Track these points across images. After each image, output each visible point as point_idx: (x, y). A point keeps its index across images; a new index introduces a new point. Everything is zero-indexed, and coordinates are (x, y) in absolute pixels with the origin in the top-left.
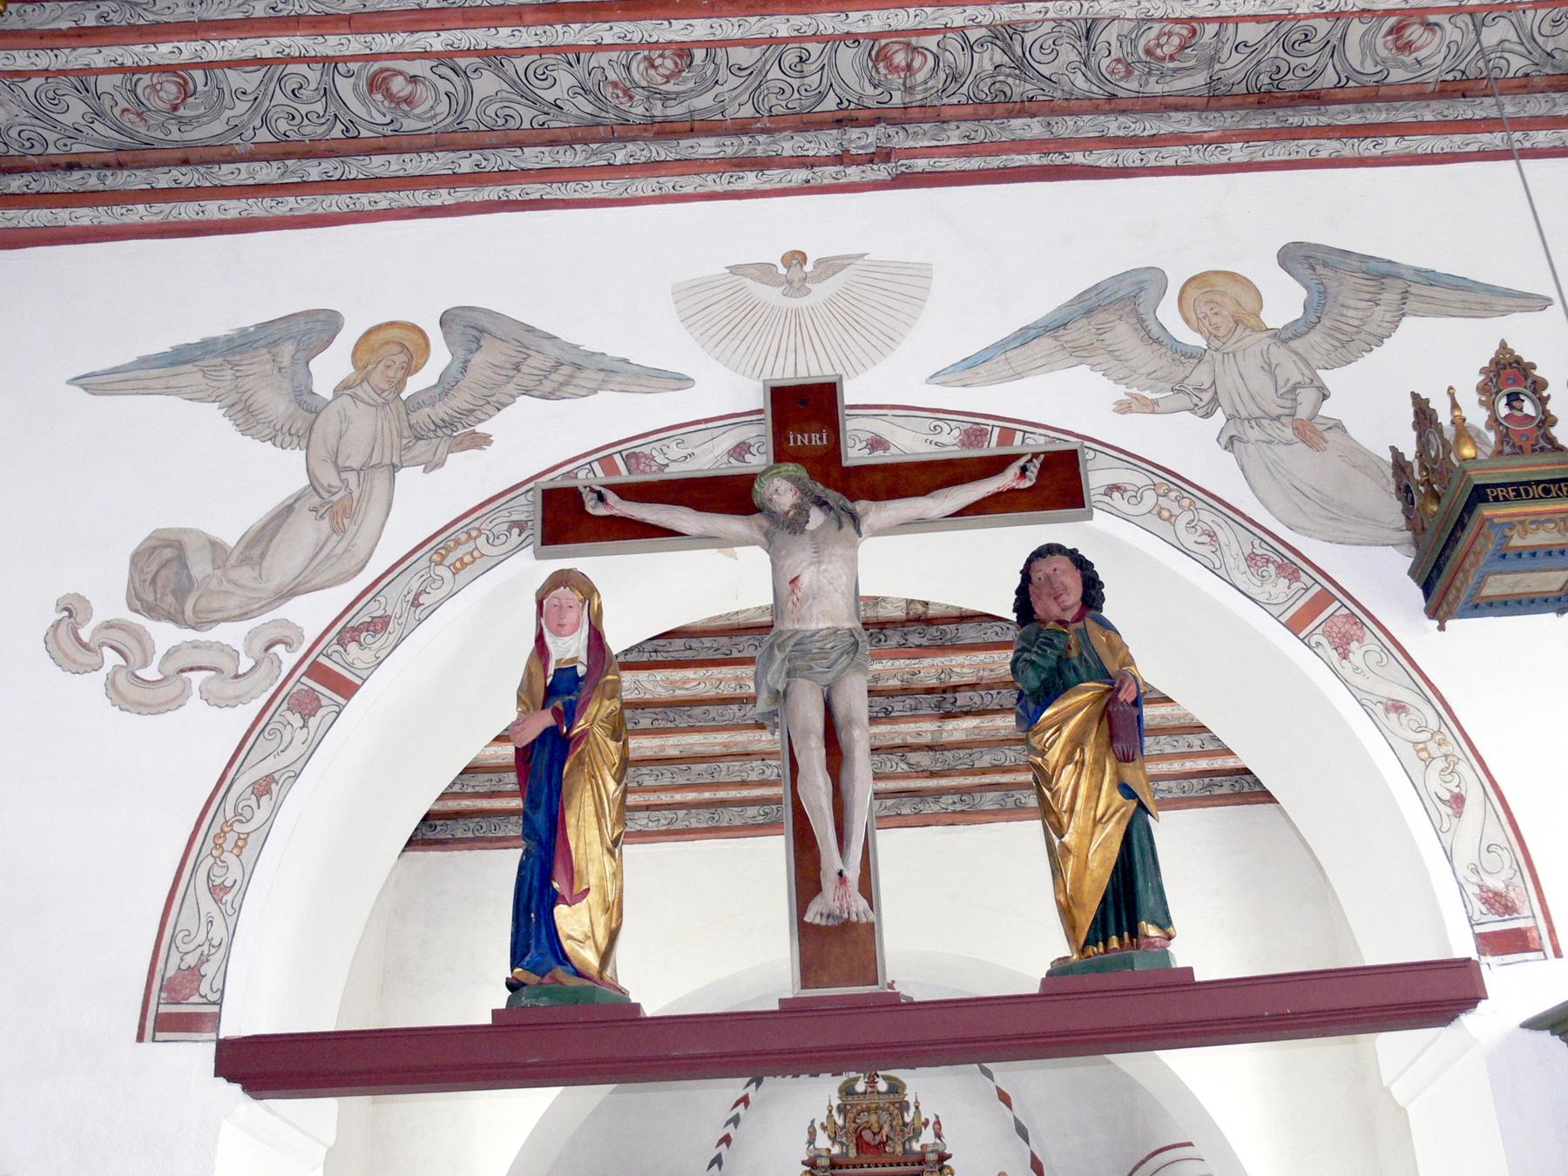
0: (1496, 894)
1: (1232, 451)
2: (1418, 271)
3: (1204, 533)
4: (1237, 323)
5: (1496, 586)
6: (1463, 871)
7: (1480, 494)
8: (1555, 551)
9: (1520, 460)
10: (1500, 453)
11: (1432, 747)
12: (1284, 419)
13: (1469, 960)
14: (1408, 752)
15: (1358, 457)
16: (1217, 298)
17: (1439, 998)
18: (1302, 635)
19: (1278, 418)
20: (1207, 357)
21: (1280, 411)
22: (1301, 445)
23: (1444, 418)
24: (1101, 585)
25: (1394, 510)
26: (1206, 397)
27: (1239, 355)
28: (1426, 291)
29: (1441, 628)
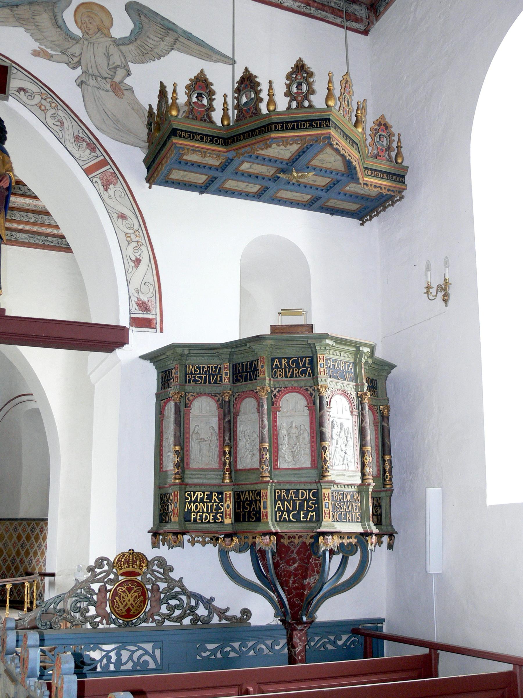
0: (143, 302)
1: (81, 88)
2: (184, 32)
3: (58, 121)
4: (99, 30)
5: (176, 175)
6: (132, 290)
7: (174, 132)
8: (202, 165)
9: (194, 122)
10: (188, 117)
11: (133, 236)
12: (107, 80)
13: (125, 327)
14: (122, 236)
15: (135, 104)
16: (93, 16)
17: (109, 340)
18: (90, 176)
19: (105, 78)
20: (81, 42)
21: (107, 76)
22: (112, 94)
23: (170, 96)
24: (6, 132)
25: (144, 132)
26: (76, 60)
27: (96, 45)
28: (186, 42)
29: (150, 187)
